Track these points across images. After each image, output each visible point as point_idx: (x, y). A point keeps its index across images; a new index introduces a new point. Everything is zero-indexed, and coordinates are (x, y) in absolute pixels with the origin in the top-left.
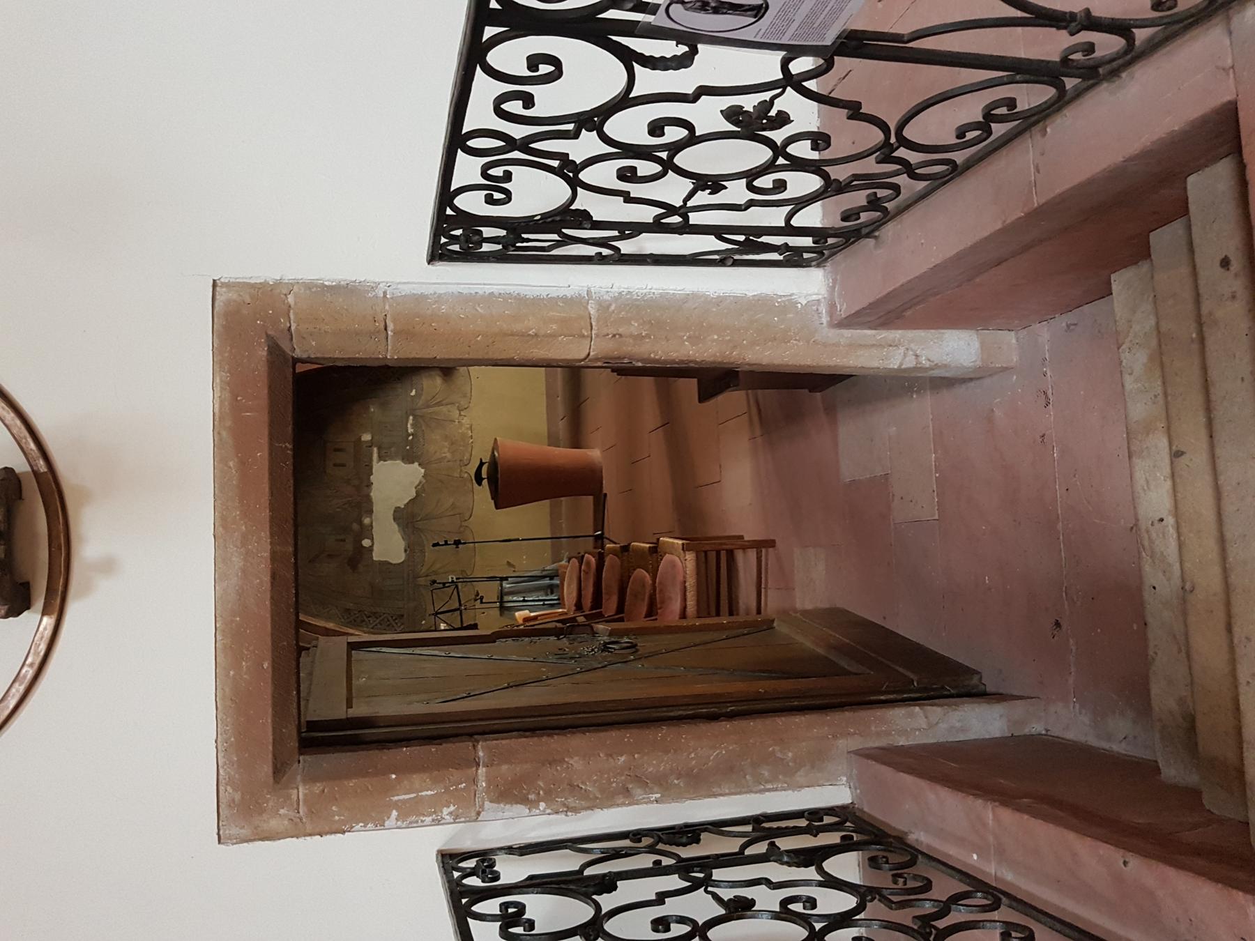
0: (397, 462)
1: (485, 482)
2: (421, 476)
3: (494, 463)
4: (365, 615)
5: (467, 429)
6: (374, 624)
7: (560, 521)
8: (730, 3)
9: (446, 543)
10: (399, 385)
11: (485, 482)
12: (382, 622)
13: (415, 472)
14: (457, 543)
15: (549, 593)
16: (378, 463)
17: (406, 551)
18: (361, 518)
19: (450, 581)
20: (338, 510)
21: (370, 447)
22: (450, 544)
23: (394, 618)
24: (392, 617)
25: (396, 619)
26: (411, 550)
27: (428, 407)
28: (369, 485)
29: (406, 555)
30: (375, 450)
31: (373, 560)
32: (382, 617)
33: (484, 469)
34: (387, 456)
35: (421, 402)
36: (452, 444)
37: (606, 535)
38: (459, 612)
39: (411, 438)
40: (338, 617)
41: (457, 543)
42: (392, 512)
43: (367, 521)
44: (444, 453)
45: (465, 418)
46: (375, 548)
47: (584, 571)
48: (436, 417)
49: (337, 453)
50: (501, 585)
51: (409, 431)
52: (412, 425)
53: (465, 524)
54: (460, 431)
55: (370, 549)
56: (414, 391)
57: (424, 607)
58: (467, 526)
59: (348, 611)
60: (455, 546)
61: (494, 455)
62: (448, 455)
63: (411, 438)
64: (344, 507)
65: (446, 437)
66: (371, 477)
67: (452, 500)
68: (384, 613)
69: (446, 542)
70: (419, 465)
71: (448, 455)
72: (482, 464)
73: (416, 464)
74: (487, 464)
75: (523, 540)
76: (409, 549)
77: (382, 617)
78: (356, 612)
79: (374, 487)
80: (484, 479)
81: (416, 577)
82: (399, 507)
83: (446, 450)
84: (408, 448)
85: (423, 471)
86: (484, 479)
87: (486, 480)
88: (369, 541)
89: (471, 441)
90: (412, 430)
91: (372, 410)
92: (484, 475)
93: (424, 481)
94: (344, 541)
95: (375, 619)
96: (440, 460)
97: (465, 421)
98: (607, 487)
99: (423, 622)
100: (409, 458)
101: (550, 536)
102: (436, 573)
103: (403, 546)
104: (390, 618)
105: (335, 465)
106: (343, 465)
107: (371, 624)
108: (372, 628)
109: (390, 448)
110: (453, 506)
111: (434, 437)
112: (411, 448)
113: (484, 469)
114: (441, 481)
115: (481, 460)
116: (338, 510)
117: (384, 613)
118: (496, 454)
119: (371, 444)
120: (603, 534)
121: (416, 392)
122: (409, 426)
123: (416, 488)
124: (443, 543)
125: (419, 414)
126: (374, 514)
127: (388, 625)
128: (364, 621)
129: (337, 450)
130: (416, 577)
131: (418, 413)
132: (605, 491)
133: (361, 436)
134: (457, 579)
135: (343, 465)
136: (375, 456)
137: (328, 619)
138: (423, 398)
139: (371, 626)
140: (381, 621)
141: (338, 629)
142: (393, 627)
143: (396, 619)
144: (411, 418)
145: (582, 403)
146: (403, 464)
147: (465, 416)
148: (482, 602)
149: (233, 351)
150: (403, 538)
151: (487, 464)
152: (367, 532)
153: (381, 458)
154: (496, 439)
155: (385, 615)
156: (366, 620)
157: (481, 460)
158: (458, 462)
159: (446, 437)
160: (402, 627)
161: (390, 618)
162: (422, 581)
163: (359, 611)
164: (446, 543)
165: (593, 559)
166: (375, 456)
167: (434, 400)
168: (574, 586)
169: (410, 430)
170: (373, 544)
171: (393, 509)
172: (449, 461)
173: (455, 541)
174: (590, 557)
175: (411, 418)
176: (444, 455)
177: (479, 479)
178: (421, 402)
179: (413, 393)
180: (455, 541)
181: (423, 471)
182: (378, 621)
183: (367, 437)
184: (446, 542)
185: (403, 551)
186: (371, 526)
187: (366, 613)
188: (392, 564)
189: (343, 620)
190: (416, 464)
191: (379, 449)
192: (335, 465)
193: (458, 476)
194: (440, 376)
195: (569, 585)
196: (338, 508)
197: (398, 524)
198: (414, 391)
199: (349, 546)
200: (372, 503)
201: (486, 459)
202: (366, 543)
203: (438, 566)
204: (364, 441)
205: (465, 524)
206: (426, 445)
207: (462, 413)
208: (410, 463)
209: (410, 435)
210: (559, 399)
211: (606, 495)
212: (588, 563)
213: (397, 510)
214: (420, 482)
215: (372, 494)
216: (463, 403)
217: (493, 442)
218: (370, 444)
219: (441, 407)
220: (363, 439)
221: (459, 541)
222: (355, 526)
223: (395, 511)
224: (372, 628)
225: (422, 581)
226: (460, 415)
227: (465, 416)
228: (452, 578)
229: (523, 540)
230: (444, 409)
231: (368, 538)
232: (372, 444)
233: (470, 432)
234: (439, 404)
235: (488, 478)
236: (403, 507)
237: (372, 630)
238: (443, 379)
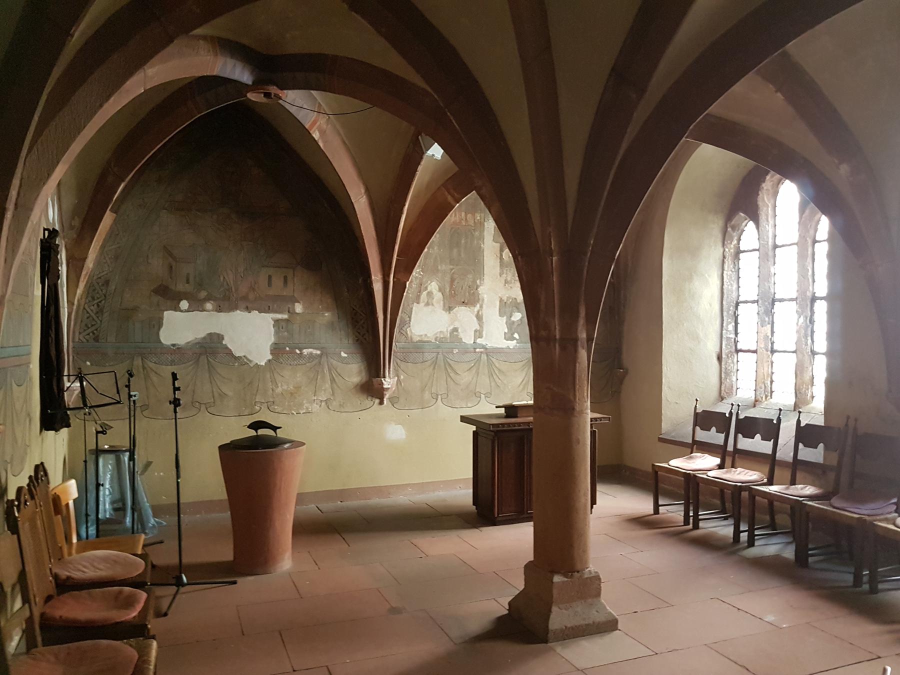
0: (273, 339)
1: (252, 433)
2: (257, 362)
3: (275, 443)
5: (307, 408)
6: (89, 310)
7: (203, 511)
8: (495, 524)
9: (176, 389)
10: (351, 341)
11: (252, 433)
12: (91, 318)
13: (261, 355)
14: (176, 403)
15: (115, 505)
17: (174, 345)
18: (213, 300)
19: (132, 393)
20: (222, 278)
21: (289, 312)
22: (175, 394)
23: (95, 332)
24: (96, 330)
25: (94, 333)
26: (174, 350)
27: (330, 370)
28: (248, 309)
29: (168, 346)
30: (285, 316)
31: (164, 311)
32: (96, 319)
33: (269, 432)
34: (279, 328)
35: (334, 362)
36: (292, 394)
37: (182, 589)
38: (82, 406)
39: (298, 352)
40: (100, 273)
41: (176, 403)
42: (217, 332)
43: (209, 306)
44: (282, 385)
45: (318, 407)
47: (120, 592)
48: (319, 377)
49: (283, 279)
50: (126, 451)
51: (304, 351)
52: (311, 353)
53: (203, 407)
54: (304, 402)
55: (177, 308)
56: (346, 355)
57: (107, 364)
58: (200, 410)
59: (107, 283)
60: (172, 400)
61: (285, 443)
62: (279, 390)
63: (298, 352)
64: (225, 283)
65: (298, 388)
66: (257, 312)
67: (230, 394)
68: (101, 321)
69: (178, 389)
70: (269, 361)
71: (279, 390)
72: (275, 429)
73: (270, 357)
74: (275, 435)
75: (178, 483)
76: (176, 350)
77: (96, 319)
78: (104, 291)
79: (246, 314)
80: (257, 432)
81: (143, 357)
83: (285, 387)
84: (288, 349)
85: (263, 363)
86: (257, 432)
87: (255, 434)
88: (186, 308)
89: (295, 413)
90: (305, 353)
91: (326, 315)
92: (261, 432)
93: (252, 365)
94: (188, 282)
95: (95, 311)
96: (274, 382)
97: (315, 407)
98: (246, 583)
99: (88, 363)
100: (277, 350)
101: (181, 501)
102: (147, 377)
103: (179, 343)
104: (94, 328)
105: (270, 277)
106: (270, 284)
107: (89, 307)
108: (84, 308)
109: (288, 332)
110: (223, 395)
111: (298, 375)
112: (287, 353)
113: (269, 432)
114: (250, 383)
115: (280, 428)
116: (222, 278)
117: (101, 321)
118: (286, 446)
119: (291, 312)
120: (183, 585)
121: (345, 357)
122: (310, 350)
123: (244, 356)
124: (177, 386)
125: (323, 360)
126: (215, 313)
127: (86, 325)
128: (93, 299)
129: (285, 278)
130: (143, 357)
131: (324, 359)
132: (240, 580)
133: (299, 302)
134: (134, 401)
135: (270, 284)
136: (279, 316)
137: (98, 263)
138: (339, 364)
139: (86, 306)
140: (92, 317)
141: (84, 273)
142: (85, 330)
143: (94, 333)
144: (319, 352)
145: (340, 534)
146: (270, 343)
147: (320, 406)
148: (98, 432)
149: (178, 402)
150: (188, 343)
151: (275, 435)
152: (197, 305)
153: (277, 322)
154: (304, 444)
155: (99, 322)
156: (96, 302)
157: (280, 428)
158: (271, 400)
159: (298, 388)
160: (85, 340)
161: (94, 328)
162: (138, 362)
164: (176, 389)
165: (135, 614)
166: (279, 316)
167: (336, 376)
168: (103, 572)
169: (305, 351)
170: (182, 311)
171: (222, 333)
172: (273, 390)
173: (179, 400)
174: (139, 607)
175: (319, 352)
176: (280, 385)
177: (256, 425)
178: (334, 362)
179: (343, 355)
180: (179, 400)
181: (263, 363)
182: (93, 315)
183: (299, 308)
184: (178, 389)
185: (174, 343)
186: (204, 310)
187: (103, 302)
188: (159, 329)
189: (95, 278)
190: (270, 357)
191: (287, 321)
192: (270, 277)
193: (257, 400)
194: (361, 380)
195: (105, 559)
196: (224, 278)
197: (204, 338)
198: (346, 355)
199: (181, 287)
200: (229, 312)
201: (280, 434)
202: (184, 304)
203: (155, 378)
204: (294, 305)
205: (203, 407)
206: (290, 367)
207: (323, 404)
208: (271, 350)
209: (300, 351)
210: (339, 502)
211: (235, 583)
212: (129, 603)
213: (220, 337)
214: (250, 361)
215: (238, 312)
216: (335, 404)
217: (279, 426)
218: (291, 312)
219: (329, 381)
220: (296, 304)
221: (179, 405)
222: (203, 294)
223: (218, 334)
224: (84, 308)
225: (138, 362)
226: (321, 401)
227: (320, 406)
228: (135, 396)
229: (178, 483)
230: (328, 385)
231: (189, 306)
232: (292, 313)
233: (304, 411)
234: (333, 380)
235: (257, 436)
236: (224, 343)
237: (82, 308)
238: (358, 385)
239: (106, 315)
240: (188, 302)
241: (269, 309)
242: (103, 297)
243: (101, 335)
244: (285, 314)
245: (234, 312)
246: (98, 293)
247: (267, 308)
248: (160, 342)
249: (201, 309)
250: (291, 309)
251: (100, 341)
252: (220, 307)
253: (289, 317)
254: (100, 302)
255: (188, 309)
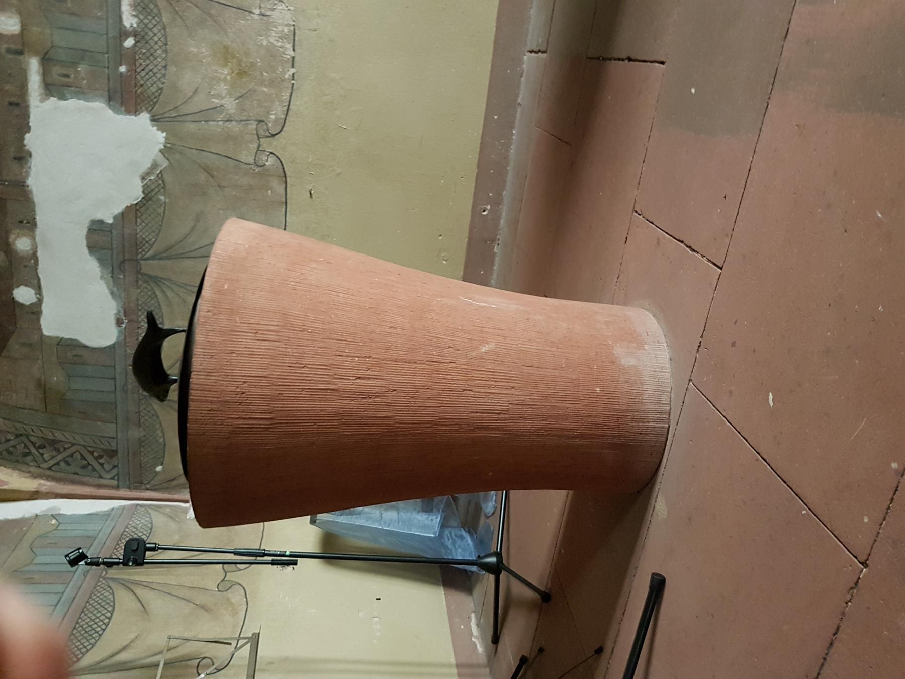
4: (34, 444)
16: (42, 101)
21: (21, 53)
31: (42, 335)
46: (45, 308)
66: (27, 136)
68: (73, 444)
82: (101, 222)
117: (73, 444)
150: (112, 293)
163: (17, 436)
170: (40, 301)
186: (34, 256)
187: (32, 439)
191: (46, 61)
218: (19, 47)
239: (59, 435)
240: (18, 286)
241: (17, 104)
242: (23, 438)
243: (102, 446)
244: (28, 64)
245: (31, 192)
246: (14, 446)
247: (16, 111)
248: (112, 347)
249: (32, 261)
250: (13, 46)
251: (114, 448)
252: (21, 222)
253: (36, 53)
254: (34, 444)
255: (32, 287)
